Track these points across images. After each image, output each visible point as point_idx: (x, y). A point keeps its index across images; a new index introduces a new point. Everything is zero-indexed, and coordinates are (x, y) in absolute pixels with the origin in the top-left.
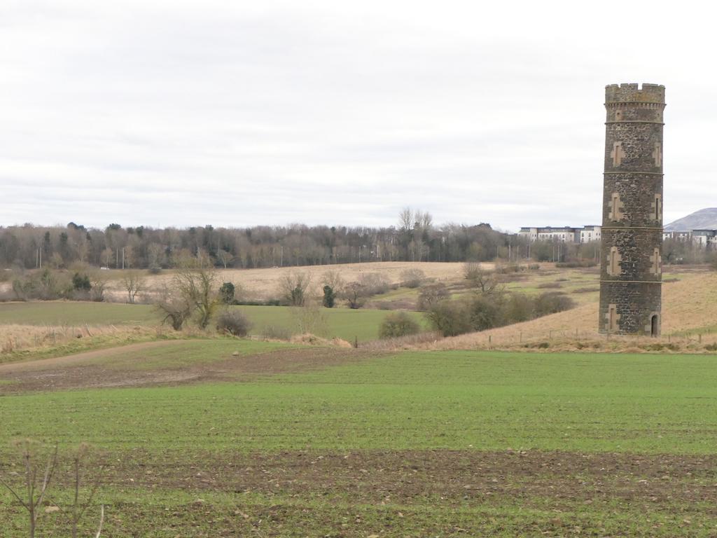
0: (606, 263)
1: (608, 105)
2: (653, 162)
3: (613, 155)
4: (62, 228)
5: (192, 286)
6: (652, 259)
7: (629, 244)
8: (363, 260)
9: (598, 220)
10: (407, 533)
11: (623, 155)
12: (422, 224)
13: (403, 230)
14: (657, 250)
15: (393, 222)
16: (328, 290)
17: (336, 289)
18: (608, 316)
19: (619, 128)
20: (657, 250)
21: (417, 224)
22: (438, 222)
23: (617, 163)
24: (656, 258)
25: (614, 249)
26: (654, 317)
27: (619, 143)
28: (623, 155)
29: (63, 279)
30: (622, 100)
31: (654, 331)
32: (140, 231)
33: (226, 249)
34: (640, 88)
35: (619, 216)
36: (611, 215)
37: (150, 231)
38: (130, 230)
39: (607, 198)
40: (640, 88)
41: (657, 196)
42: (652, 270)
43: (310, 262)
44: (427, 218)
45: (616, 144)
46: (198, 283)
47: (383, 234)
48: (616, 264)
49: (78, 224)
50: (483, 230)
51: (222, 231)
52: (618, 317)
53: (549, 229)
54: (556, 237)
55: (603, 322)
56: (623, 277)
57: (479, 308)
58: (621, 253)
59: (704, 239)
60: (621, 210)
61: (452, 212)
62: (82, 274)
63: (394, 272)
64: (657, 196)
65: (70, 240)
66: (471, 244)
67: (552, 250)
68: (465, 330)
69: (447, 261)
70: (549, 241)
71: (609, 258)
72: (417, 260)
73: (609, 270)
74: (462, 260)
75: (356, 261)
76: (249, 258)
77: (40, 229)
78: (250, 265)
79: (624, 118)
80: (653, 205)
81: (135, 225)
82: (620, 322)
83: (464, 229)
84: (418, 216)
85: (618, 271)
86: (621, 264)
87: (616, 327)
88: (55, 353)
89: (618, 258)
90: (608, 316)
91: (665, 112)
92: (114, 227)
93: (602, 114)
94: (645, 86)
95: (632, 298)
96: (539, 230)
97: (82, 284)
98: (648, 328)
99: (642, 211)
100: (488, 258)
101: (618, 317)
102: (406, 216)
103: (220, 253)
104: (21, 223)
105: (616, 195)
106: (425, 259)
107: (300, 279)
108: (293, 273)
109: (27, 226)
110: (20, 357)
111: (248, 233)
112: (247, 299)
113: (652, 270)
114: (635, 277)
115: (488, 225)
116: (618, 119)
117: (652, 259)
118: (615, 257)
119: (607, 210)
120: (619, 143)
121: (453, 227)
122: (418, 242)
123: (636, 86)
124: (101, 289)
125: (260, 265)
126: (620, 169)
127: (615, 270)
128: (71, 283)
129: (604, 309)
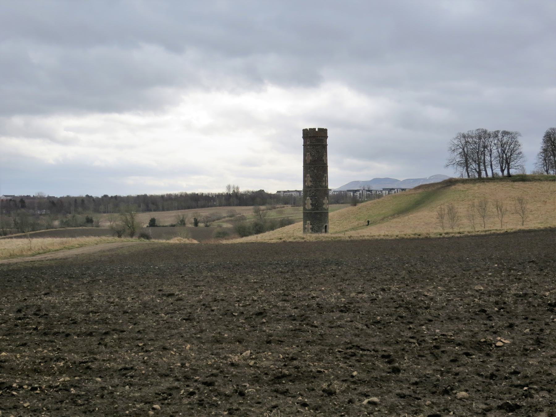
0: (305, 204)
1: (304, 137)
2: (323, 161)
3: (307, 158)
4: (82, 197)
5: (127, 219)
6: (324, 201)
7: (315, 196)
8: (211, 206)
9: (300, 187)
10: (195, 342)
11: (311, 158)
12: (236, 191)
13: (227, 193)
14: (326, 198)
15: (222, 190)
16: (196, 220)
17: (199, 219)
18: (307, 226)
19: (308, 147)
20: (326, 198)
21: (234, 191)
22: (242, 190)
23: (308, 162)
24: (326, 201)
25: (308, 198)
26: (326, 226)
27: (309, 153)
28: (311, 158)
29: (81, 218)
30: (309, 135)
31: (326, 231)
32: (116, 197)
33: (153, 204)
34: (317, 130)
35: (310, 184)
36: (306, 184)
37: (120, 197)
38: (112, 197)
39: (305, 176)
40: (317, 130)
41: (325, 175)
42: (324, 206)
43: (189, 208)
44: (238, 188)
45: (308, 154)
46: (129, 217)
47: (219, 196)
48: (309, 204)
49: (90, 195)
50: (261, 193)
51: (151, 196)
52: (311, 226)
53: (288, 191)
54: (291, 195)
55: (305, 229)
56: (312, 210)
57: (256, 225)
58: (311, 199)
59: (352, 194)
60: (311, 181)
61: (247, 186)
62: (90, 216)
63: (224, 211)
64: (325, 175)
65: (86, 202)
66: (258, 198)
67: (283, 199)
68: (250, 234)
69: (246, 206)
70: (289, 196)
71: (306, 202)
72: (234, 206)
73: (307, 207)
74: (252, 205)
75: (208, 207)
76: (163, 207)
77: (73, 197)
78: (163, 210)
79: (311, 142)
80: (324, 179)
81: (114, 195)
82: (312, 229)
83: (253, 192)
84: (233, 187)
85: (310, 207)
86: (311, 204)
87: (310, 231)
88: (33, 255)
89: (310, 201)
90: (307, 226)
91: (328, 140)
92: (106, 196)
93: (302, 141)
94: (319, 129)
95: (316, 218)
96: (284, 192)
97: (89, 221)
98: (324, 230)
99: (320, 182)
100: (263, 204)
101: (311, 226)
102: (229, 187)
103: (150, 206)
104: (65, 196)
105: (308, 175)
106: (237, 205)
107: (183, 215)
108: (180, 213)
109: (68, 197)
110: (22, 256)
111: (162, 197)
112: (161, 225)
113: (324, 206)
114: (317, 210)
115: (263, 191)
116: (308, 143)
117: (324, 201)
118: (309, 201)
119: (305, 181)
120: (309, 153)
121: (248, 192)
122: (235, 199)
123: (315, 129)
124: (98, 222)
125: (168, 210)
126: (310, 164)
127: (309, 207)
128: (85, 220)
129: (305, 223)
